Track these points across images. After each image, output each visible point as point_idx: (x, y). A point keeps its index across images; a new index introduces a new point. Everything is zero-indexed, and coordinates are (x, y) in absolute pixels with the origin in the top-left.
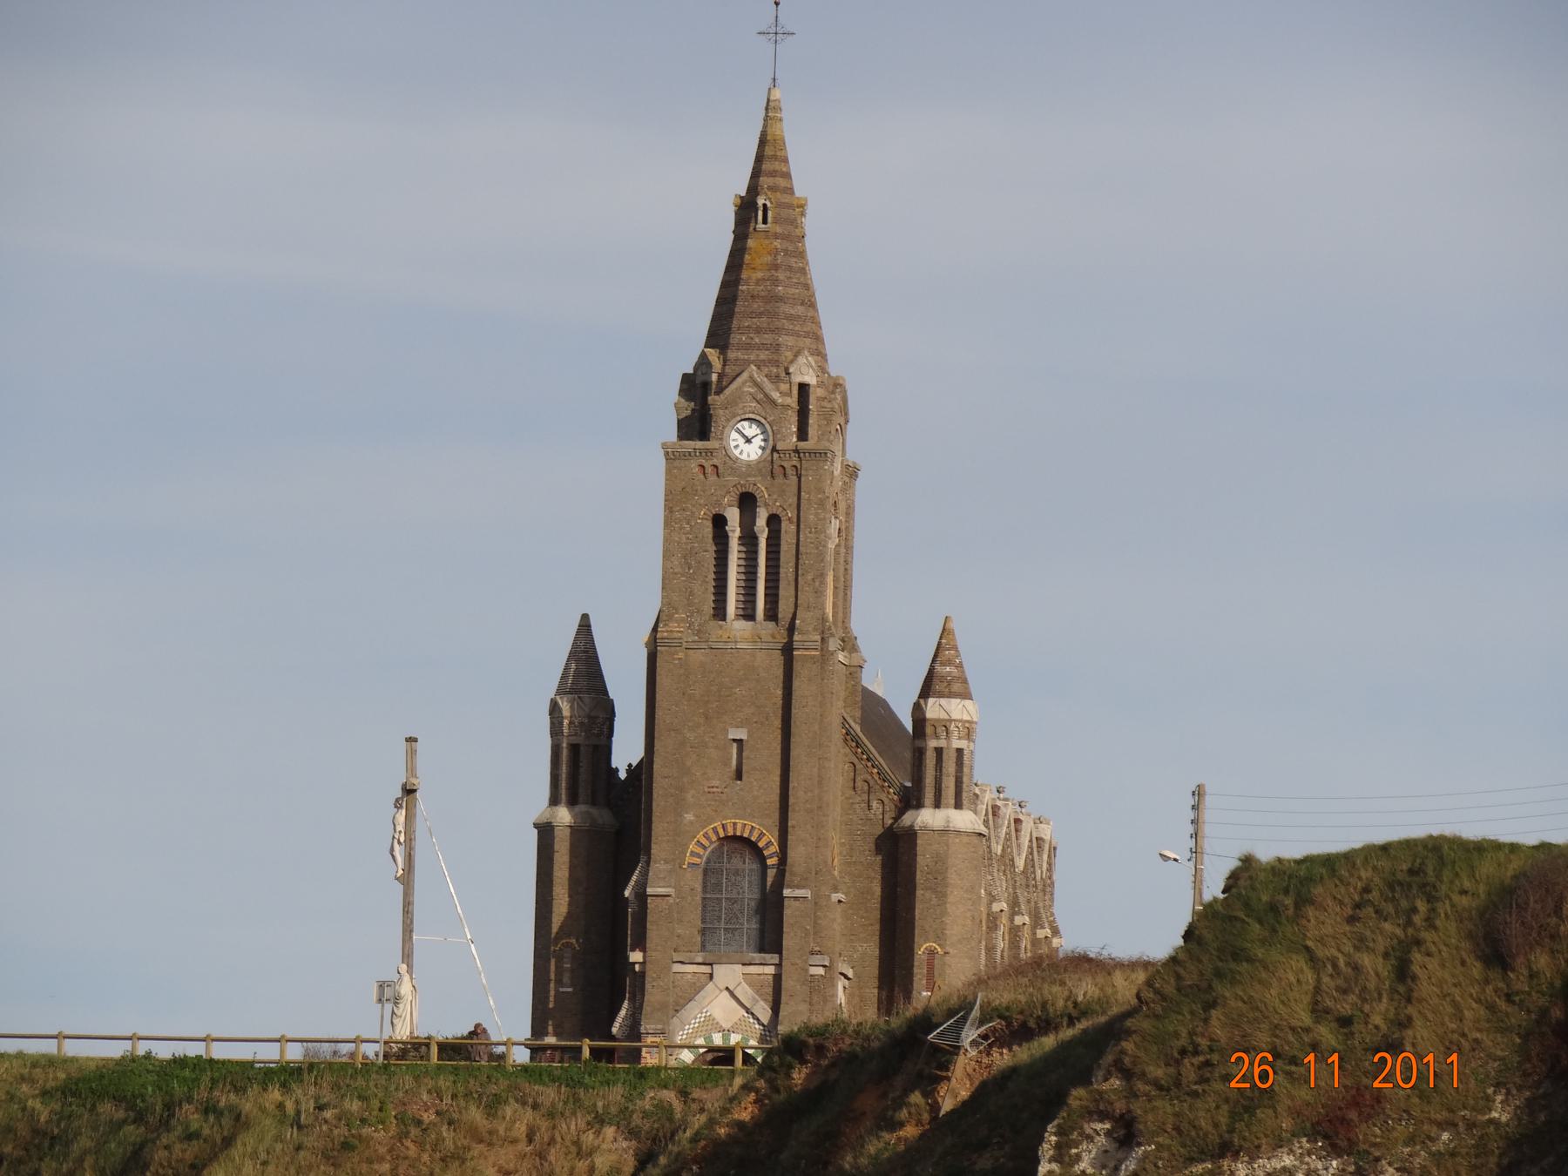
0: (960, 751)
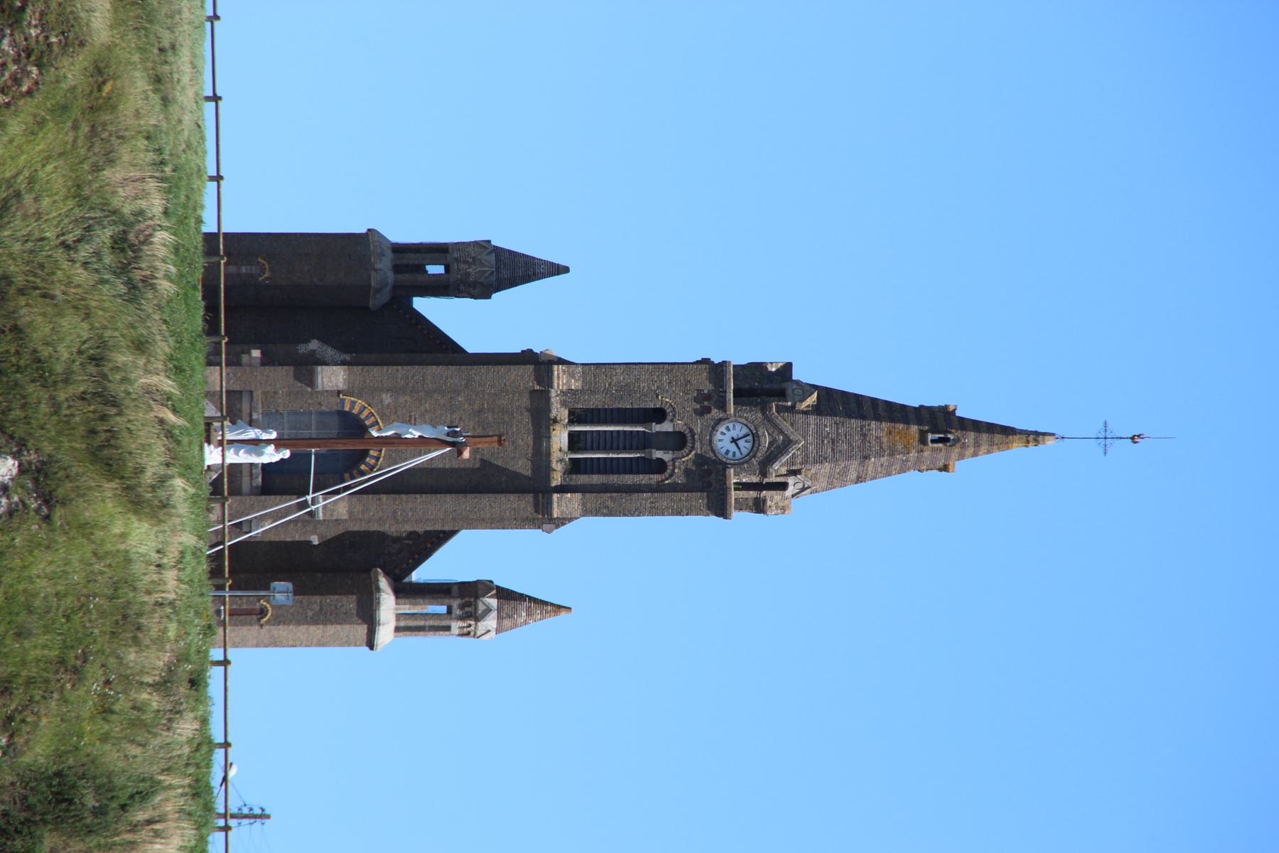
0: (448, 628)
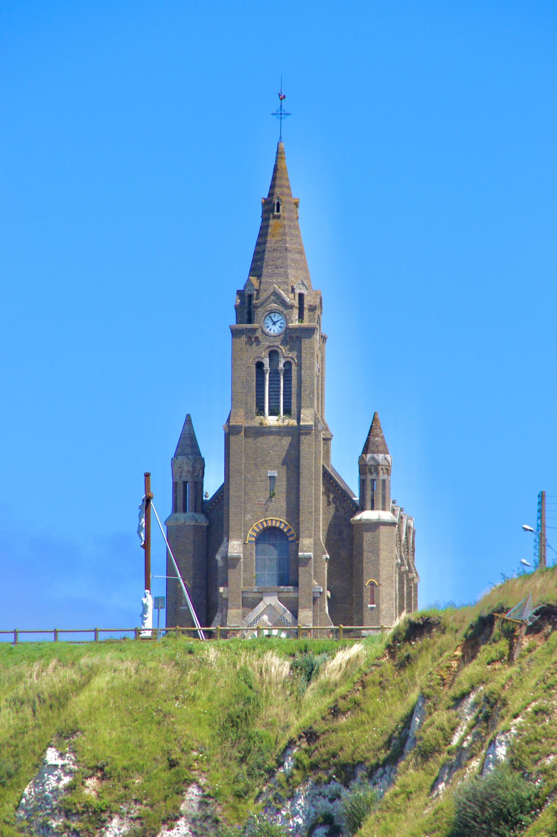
0: (384, 481)
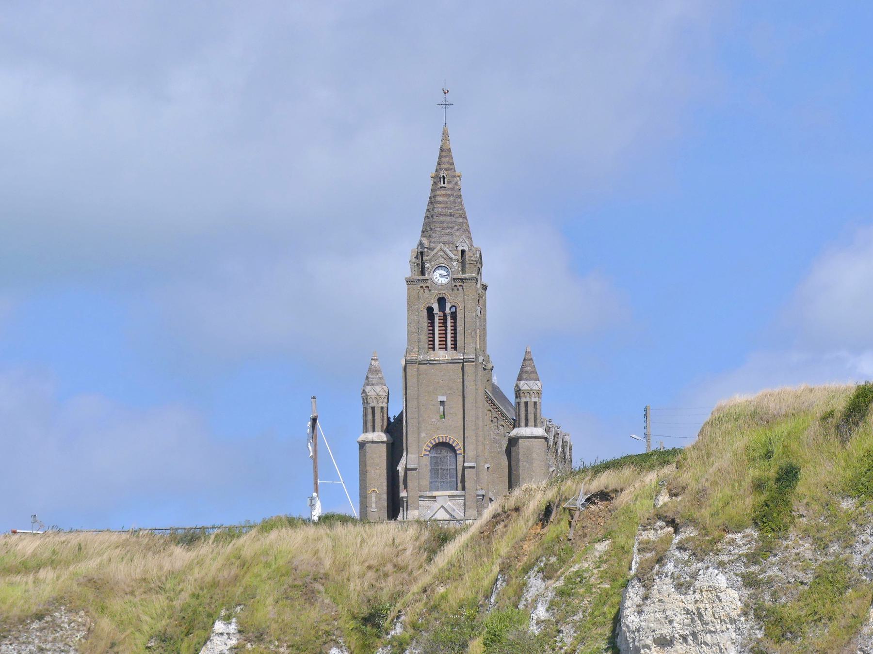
0: (535, 403)
